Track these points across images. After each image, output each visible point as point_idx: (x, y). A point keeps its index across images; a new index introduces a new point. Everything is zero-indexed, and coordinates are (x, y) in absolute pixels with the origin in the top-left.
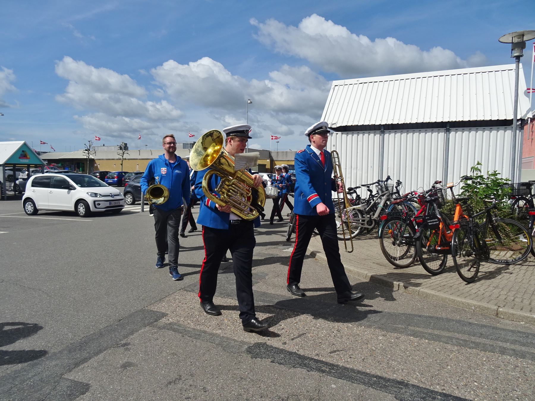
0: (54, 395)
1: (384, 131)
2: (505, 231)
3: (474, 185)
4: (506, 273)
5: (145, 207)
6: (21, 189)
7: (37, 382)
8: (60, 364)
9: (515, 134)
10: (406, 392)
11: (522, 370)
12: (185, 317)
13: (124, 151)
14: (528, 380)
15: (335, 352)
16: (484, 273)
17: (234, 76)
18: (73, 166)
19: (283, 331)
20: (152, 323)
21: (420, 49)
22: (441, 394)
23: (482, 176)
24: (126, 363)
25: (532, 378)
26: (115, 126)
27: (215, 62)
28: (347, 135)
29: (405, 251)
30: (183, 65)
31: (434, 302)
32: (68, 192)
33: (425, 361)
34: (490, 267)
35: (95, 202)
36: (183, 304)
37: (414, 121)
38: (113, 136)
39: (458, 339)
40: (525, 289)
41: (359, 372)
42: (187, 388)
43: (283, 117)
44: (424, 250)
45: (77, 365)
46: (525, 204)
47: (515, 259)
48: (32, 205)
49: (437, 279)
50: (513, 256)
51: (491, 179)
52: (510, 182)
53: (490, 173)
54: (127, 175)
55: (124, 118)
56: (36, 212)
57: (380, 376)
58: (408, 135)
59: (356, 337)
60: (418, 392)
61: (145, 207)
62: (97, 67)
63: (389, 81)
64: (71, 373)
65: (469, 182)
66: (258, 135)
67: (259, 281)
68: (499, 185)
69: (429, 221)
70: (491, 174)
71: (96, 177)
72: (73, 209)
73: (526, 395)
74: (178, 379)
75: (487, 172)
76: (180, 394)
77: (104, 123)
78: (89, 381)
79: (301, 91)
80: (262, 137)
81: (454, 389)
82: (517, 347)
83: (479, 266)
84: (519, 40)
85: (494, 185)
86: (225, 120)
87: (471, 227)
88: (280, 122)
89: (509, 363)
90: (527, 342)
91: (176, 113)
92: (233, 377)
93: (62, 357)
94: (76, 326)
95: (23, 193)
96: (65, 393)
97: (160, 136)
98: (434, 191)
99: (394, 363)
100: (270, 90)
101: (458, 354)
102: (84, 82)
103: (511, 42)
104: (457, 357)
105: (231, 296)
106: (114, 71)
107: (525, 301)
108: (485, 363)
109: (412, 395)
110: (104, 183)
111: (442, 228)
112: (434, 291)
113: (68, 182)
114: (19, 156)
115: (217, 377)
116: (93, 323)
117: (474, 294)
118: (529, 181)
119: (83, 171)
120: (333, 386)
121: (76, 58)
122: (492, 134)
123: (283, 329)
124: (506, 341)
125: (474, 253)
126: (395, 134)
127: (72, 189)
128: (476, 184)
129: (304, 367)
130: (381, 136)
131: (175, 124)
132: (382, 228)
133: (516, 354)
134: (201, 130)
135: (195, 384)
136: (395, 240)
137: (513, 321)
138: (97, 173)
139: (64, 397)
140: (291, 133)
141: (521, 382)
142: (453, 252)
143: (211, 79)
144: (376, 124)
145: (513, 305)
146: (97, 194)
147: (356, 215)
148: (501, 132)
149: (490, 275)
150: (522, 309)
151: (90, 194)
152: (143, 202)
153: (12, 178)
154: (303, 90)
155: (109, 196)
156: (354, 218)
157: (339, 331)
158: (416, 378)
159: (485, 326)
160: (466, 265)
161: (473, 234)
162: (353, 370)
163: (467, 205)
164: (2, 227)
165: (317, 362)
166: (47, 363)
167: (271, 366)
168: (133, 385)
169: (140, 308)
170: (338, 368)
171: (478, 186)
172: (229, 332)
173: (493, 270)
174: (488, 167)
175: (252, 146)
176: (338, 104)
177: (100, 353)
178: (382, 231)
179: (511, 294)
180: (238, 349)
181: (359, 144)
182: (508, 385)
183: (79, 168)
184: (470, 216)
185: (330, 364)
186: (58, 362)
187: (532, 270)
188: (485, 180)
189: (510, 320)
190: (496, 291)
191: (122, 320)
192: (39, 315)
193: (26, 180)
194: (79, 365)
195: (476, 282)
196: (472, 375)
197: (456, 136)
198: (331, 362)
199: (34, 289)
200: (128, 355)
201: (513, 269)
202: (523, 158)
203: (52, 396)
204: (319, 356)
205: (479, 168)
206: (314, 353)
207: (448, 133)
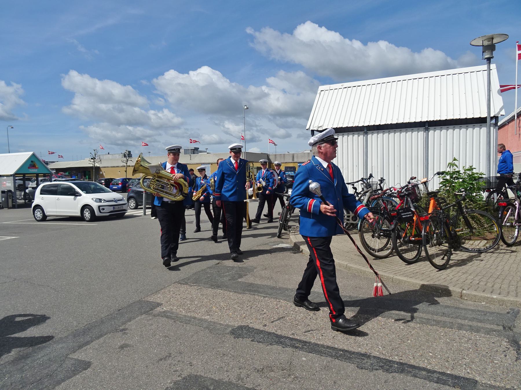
1: (368, 132)
2: (480, 222)
3: (452, 179)
4: (477, 260)
5: (147, 210)
6: (31, 197)
7: (46, 361)
8: (66, 347)
9: (489, 131)
10: (367, 362)
11: (474, 342)
12: (177, 306)
13: (128, 158)
15: (309, 331)
16: (456, 261)
18: (79, 175)
19: (265, 315)
20: (148, 311)
22: (397, 363)
23: (459, 171)
24: (124, 344)
25: (481, 348)
26: (119, 135)
27: (214, 70)
30: (183, 74)
32: (74, 198)
33: (389, 337)
34: (463, 256)
35: (99, 207)
36: (176, 295)
37: (395, 122)
38: (118, 145)
39: (422, 318)
40: (491, 274)
41: (328, 347)
43: (280, 121)
45: (80, 347)
47: (486, 248)
48: (41, 212)
49: (412, 268)
51: (467, 173)
54: (131, 181)
55: (128, 127)
56: (44, 218)
57: (346, 350)
58: (390, 135)
61: (146, 211)
62: (100, 79)
63: (381, 84)
64: (75, 353)
65: (448, 177)
66: (257, 139)
67: (247, 273)
69: (403, 214)
72: (79, 214)
73: (473, 362)
74: (168, 356)
77: (108, 132)
78: (91, 359)
79: (297, 95)
80: (261, 140)
81: (410, 359)
82: (475, 324)
84: (489, 43)
85: (470, 179)
86: (224, 125)
87: (441, 218)
88: (277, 125)
91: (177, 120)
92: (216, 354)
95: (33, 201)
97: (163, 143)
98: (412, 187)
99: (360, 339)
100: (266, 95)
101: (419, 331)
102: (89, 94)
103: (482, 45)
104: (418, 333)
105: (220, 287)
109: (372, 364)
110: (108, 189)
111: (416, 220)
113: (74, 189)
114: (28, 166)
115: (203, 354)
117: (443, 279)
119: (90, 179)
120: (304, 359)
121: (81, 72)
122: (468, 131)
124: (465, 318)
126: (378, 134)
127: (77, 196)
129: (280, 344)
130: (364, 137)
131: (177, 131)
132: (361, 222)
133: (471, 329)
134: (202, 136)
136: (374, 233)
137: (476, 301)
138: (102, 180)
139: (69, 373)
140: (288, 136)
141: (471, 352)
143: (211, 86)
144: (360, 126)
145: (477, 287)
148: (477, 129)
149: (462, 263)
151: (94, 199)
152: (145, 206)
153: (22, 188)
154: (298, 94)
155: (113, 201)
157: (315, 314)
162: (323, 346)
163: (437, 198)
164: (14, 233)
166: (55, 346)
167: (251, 344)
169: (138, 299)
170: (310, 344)
171: (456, 181)
173: (466, 258)
175: (252, 149)
177: (101, 337)
178: (361, 225)
183: (85, 176)
185: (304, 341)
186: (64, 345)
187: (502, 257)
188: (461, 175)
189: (472, 301)
190: (464, 276)
192: (47, 307)
193: (35, 189)
195: (447, 269)
196: (429, 347)
197: (435, 134)
198: (305, 340)
199: (42, 286)
201: (484, 256)
203: (58, 372)
204: (294, 335)
206: (290, 333)
207: (427, 132)
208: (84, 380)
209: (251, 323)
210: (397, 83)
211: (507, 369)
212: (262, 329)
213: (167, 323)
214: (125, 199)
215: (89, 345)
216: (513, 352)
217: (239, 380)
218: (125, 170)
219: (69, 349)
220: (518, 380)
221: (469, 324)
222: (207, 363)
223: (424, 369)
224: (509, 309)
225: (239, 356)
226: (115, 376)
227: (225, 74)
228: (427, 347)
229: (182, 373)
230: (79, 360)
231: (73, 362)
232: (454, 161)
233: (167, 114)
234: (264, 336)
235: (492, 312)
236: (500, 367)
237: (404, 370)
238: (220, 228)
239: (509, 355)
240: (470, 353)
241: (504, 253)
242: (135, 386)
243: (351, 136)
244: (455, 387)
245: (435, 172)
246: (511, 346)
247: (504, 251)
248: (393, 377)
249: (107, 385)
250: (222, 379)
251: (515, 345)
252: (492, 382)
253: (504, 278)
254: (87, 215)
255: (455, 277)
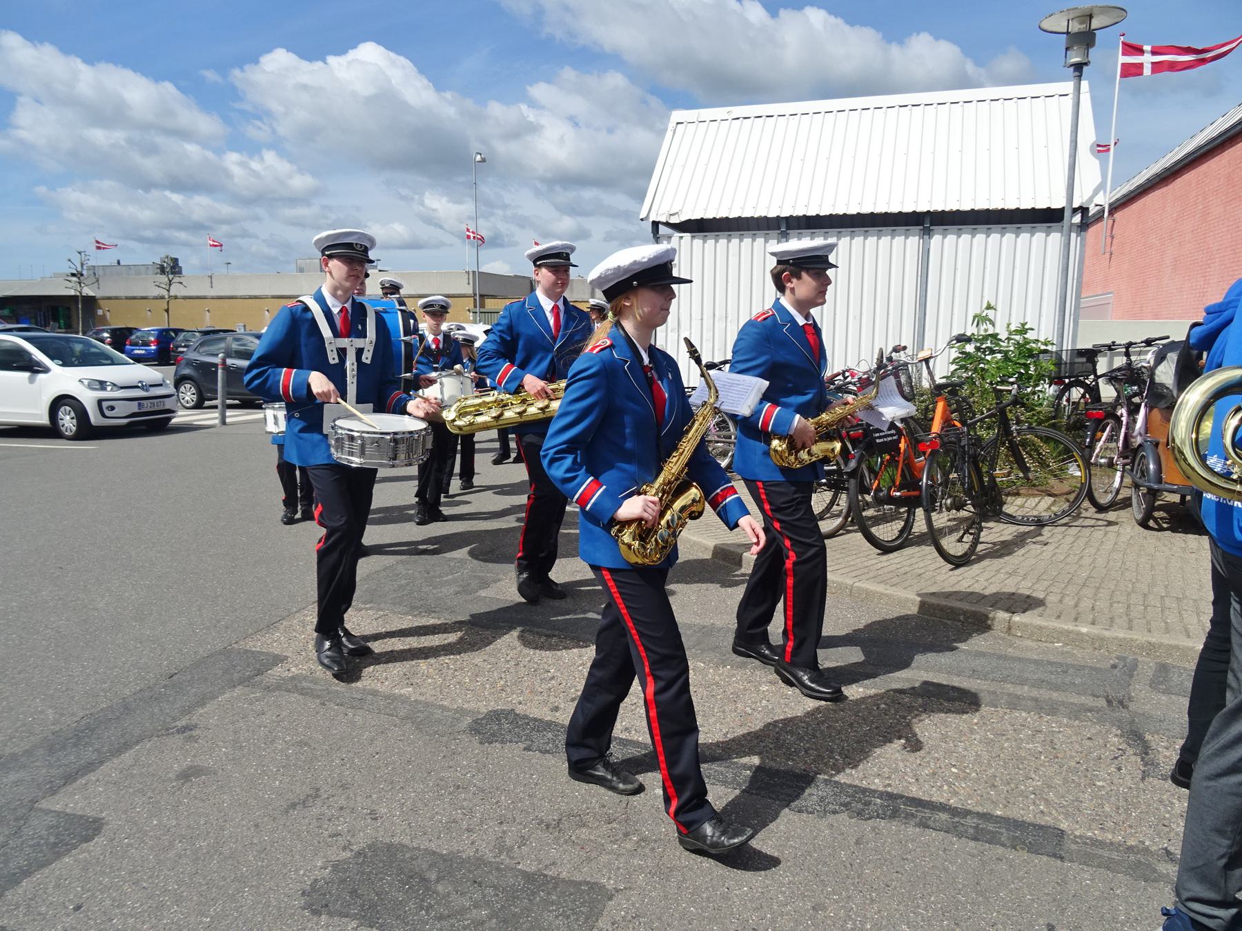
0: (17, 847)
1: (788, 231)
2: (1040, 454)
3: (979, 354)
4: (1034, 543)
8: (29, 779)
9: (1067, 241)
11: (1048, 739)
13: (171, 276)
14: (1057, 758)
16: (990, 545)
17: (443, 94)
19: (553, 682)
21: (884, 38)
22: (882, 795)
23: (997, 334)
24: (190, 768)
26: (146, 215)
27: (392, 55)
28: (705, 239)
29: (828, 502)
31: (882, 608)
33: (856, 731)
34: (1003, 532)
35: (100, 402)
38: (143, 240)
40: (1070, 576)
42: (333, 815)
43: (565, 196)
44: (868, 498)
45: (69, 778)
46: (1083, 396)
47: (1055, 514)
49: (892, 561)
50: (1053, 508)
51: (1015, 340)
52: (1054, 349)
53: (1013, 328)
55: (168, 193)
59: (713, 689)
60: (835, 794)
62: (90, 60)
64: (57, 797)
65: (970, 348)
66: (506, 240)
67: (501, 576)
68: (1030, 353)
70: (1014, 331)
71: (103, 342)
72: (44, 420)
73: (1050, 787)
75: (1006, 325)
76: (318, 827)
77: (116, 207)
80: (515, 244)
81: (910, 783)
82: (1044, 694)
83: (981, 529)
85: (1020, 354)
87: (964, 446)
88: (558, 208)
89: (1024, 726)
90: (1064, 683)
91: (300, 182)
92: (438, 785)
93: (33, 762)
94: (64, 692)
96: (42, 842)
97: (263, 241)
98: (893, 369)
100: (534, 129)
102: (66, 100)
103: (1066, 31)
106: (135, 71)
107: (1066, 600)
108: (976, 728)
109: (822, 799)
110: (123, 356)
111: (905, 450)
112: (882, 585)
113: (29, 354)
115: (402, 788)
116: (105, 683)
118: (1094, 346)
123: (553, 678)
124: (1023, 682)
125: (969, 502)
126: (852, 238)
127: (38, 372)
128: (984, 353)
131: (301, 212)
133: (1039, 706)
135: (351, 804)
138: (103, 331)
139: (41, 851)
141: (1044, 762)
142: (925, 500)
143: (385, 98)
144: (770, 215)
146: (106, 382)
147: (724, 425)
148: (1039, 236)
149: (1003, 549)
150: (1059, 617)
151: (86, 382)
152: (223, 402)
154: (610, 131)
155: (137, 387)
156: (720, 430)
158: (834, 764)
159: (983, 654)
160: (952, 530)
161: (968, 462)
165: (625, 745)
168: (207, 815)
169: (219, 646)
171: (989, 358)
172: (432, 690)
173: (1009, 538)
174: (1010, 315)
176: (684, 166)
177: (126, 749)
179: (1071, 590)
180: (451, 727)
181: (730, 262)
182: (1019, 768)
183: (56, 319)
184: (964, 423)
186: (22, 774)
187: (1088, 535)
188: (1001, 343)
189: (1033, 640)
191: (176, 674)
194: (76, 778)
196: (949, 752)
197: (944, 244)
200: (194, 751)
201: (1049, 534)
202: (1082, 296)
203: (12, 849)
204: (630, 732)
205: (991, 317)
207: (926, 237)
208: (85, 869)
209: (520, 703)
210: (812, 117)
211: (1126, 800)
212: (548, 718)
213: (303, 709)
214: (170, 382)
215: (92, 774)
216: (1133, 758)
217: (501, 853)
218: (166, 307)
219: (38, 784)
220: (1150, 826)
221: (1032, 695)
222: (414, 810)
223: (943, 808)
224: (1116, 658)
225: (497, 789)
226: (171, 854)
227: (423, 67)
228: (945, 753)
229: (353, 841)
230: (67, 815)
231: (51, 821)
232: (986, 311)
233: (271, 164)
234: (556, 736)
235: (1080, 666)
236: (1111, 797)
237: (897, 811)
238: (456, 475)
239: (1126, 768)
240: (1041, 765)
241: (1093, 526)
242: (229, 880)
243: (723, 242)
244: (1016, 850)
245: (955, 333)
246: (1130, 745)
247: (1092, 522)
248: (874, 829)
249: (150, 880)
250: (459, 851)
251: (1136, 741)
252: (1096, 832)
253: (1097, 585)
254: (68, 421)
255: (991, 583)
